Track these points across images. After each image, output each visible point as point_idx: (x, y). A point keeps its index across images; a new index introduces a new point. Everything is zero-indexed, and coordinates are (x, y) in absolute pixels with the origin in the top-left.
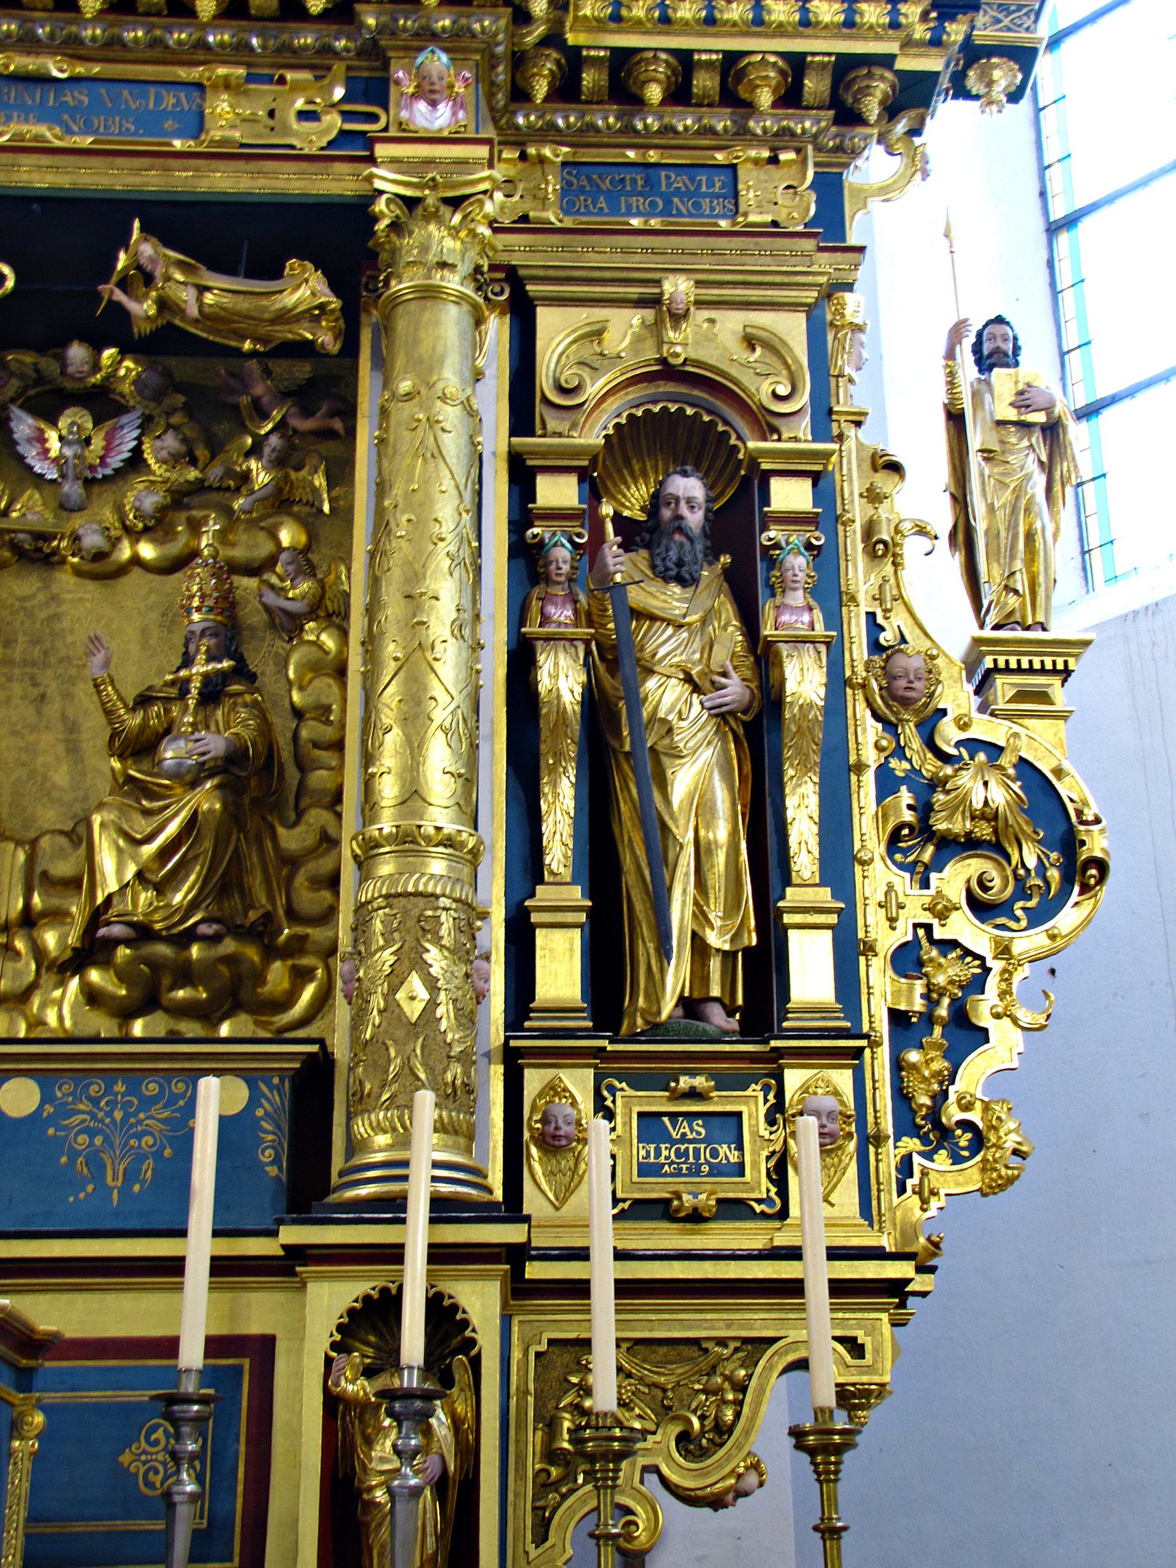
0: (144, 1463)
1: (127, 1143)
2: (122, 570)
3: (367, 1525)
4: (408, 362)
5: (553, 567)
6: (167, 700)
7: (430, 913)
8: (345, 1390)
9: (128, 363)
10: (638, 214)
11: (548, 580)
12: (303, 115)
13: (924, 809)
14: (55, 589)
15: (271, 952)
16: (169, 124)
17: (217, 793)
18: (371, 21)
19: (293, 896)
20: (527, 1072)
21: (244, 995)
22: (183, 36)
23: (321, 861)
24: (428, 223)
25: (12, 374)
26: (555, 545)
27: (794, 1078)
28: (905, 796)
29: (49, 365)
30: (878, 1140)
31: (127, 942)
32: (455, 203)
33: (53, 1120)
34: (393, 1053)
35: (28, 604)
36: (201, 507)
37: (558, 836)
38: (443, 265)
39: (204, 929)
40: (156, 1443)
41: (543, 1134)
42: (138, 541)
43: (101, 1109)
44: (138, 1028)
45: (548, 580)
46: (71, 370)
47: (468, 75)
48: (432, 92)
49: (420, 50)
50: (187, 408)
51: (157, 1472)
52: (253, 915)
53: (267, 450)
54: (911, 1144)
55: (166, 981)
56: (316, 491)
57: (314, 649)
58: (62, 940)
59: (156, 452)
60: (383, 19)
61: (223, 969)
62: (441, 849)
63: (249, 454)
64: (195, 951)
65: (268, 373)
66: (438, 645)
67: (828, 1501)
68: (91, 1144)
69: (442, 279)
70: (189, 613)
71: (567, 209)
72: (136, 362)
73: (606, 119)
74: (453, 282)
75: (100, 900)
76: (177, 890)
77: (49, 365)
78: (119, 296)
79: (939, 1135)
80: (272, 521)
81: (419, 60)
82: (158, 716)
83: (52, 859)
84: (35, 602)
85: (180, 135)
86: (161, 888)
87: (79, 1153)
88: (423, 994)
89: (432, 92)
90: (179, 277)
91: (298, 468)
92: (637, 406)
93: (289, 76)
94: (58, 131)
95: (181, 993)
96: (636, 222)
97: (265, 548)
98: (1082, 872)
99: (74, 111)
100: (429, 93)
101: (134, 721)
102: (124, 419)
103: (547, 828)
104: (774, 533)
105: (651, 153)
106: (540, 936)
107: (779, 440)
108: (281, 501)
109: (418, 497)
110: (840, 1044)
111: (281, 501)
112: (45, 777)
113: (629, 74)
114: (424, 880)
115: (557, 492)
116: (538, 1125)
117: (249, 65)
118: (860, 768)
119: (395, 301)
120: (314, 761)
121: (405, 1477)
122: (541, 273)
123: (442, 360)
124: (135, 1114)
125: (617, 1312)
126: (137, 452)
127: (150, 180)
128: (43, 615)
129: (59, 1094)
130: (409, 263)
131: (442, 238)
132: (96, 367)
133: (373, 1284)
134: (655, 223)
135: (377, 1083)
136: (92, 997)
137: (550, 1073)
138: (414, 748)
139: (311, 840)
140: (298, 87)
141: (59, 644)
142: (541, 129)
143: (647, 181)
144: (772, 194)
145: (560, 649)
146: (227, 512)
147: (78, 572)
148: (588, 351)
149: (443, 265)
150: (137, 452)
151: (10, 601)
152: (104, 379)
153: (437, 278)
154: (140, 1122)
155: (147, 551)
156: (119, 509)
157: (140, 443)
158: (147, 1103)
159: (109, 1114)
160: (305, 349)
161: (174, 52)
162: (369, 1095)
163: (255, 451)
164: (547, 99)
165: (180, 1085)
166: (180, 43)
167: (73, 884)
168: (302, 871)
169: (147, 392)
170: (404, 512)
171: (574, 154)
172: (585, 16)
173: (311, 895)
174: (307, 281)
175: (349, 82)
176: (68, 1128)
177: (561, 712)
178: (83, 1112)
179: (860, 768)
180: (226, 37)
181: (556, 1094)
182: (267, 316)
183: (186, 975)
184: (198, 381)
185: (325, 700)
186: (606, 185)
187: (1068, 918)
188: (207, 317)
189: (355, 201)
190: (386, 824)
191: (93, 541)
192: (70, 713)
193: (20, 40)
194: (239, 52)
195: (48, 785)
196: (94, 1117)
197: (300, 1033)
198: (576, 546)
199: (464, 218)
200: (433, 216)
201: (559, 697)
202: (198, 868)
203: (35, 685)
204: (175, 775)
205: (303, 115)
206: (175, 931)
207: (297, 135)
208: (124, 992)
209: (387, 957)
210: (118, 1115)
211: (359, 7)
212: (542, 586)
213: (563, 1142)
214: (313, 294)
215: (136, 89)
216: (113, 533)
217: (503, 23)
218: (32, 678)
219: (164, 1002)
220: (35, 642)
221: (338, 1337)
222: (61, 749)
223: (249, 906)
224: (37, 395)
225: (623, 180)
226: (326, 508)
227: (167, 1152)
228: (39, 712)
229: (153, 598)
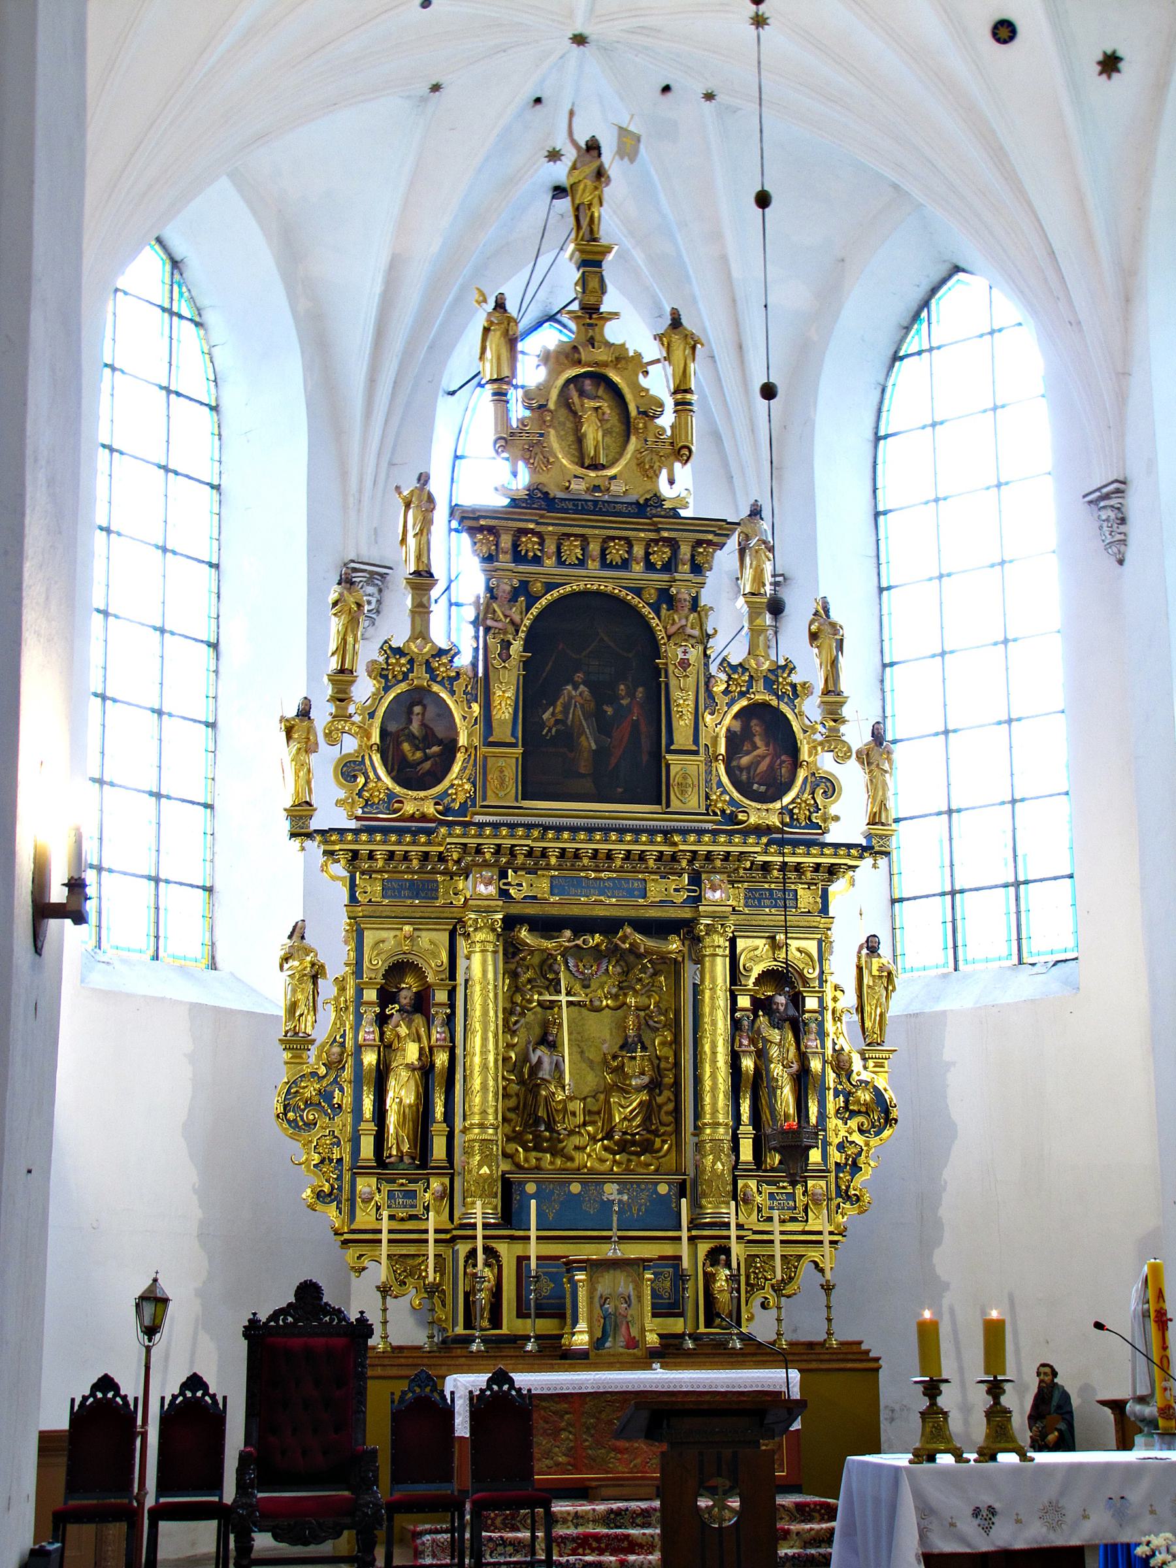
12: (676, 890)
13: (847, 1102)
27: (810, 1183)
28: (842, 1098)
30: (831, 1199)
54: (840, 1200)
67: (828, 1300)
74: (719, 951)
79: (848, 1198)
98: (889, 1121)
100: (714, 889)
103: (742, 1109)
104: (807, 1015)
110: (821, 1173)
118: (829, 1089)
127: (633, 913)
138: (714, 1098)
144: (806, 898)
158: (642, 1190)
179: (829, 1089)
187: (886, 1133)
190: (476, 1120)
205: (676, 890)
223: (652, 1124)
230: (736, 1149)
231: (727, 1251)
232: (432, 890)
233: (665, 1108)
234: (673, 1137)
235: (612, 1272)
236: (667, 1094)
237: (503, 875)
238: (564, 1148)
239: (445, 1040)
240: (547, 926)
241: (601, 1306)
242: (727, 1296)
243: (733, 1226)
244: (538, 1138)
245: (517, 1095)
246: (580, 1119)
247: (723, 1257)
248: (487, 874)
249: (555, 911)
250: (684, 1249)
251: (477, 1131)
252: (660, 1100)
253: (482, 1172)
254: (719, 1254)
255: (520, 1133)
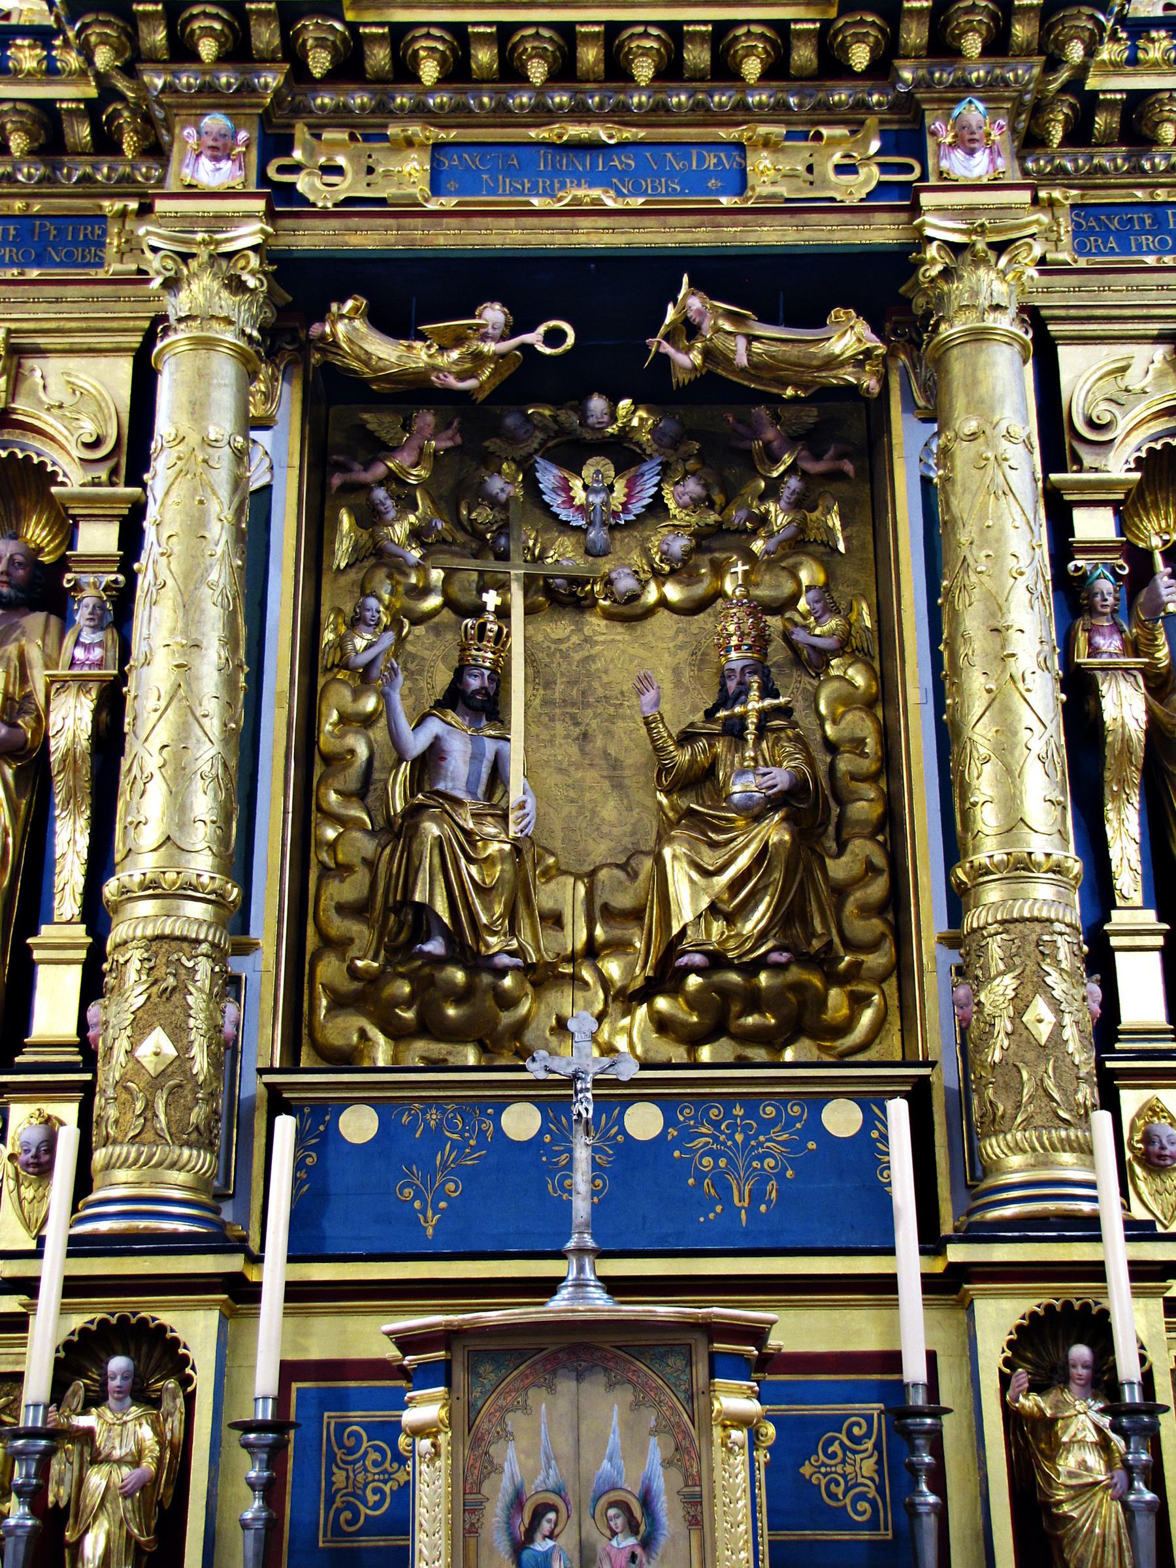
0: (825, 1475)
1: (750, 1165)
2: (650, 612)
3: (1060, 1539)
4: (969, 403)
5: (1098, 598)
6: (710, 736)
7: (1046, 938)
8: (1023, 1406)
9: (642, 413)
10: (1150, 252)
11: (1092, 611)
12: (840, 169)
14: (587, 631)
15: (834, 978)
16: (712, 183)
17: (785, 825)
18: (907, 75)
19: (845, 924)
20: (1123, 1093)
21: (808, 1019)
22: (724, 99)
23: (869, 890)
24: (977, 267)
25: (536, 427)
26: (1098, 577)
29: (570, 418)
31: (698, 971)
32: (1000, 248)
33: (677, 1143)
34: (1025, 1076)
35: (563, 647)
36: (723, 550)
37: (1125, 862)
38: (997, 308)
39: (775, 957)
40: (834, 1456)
41: (1146, 1153)
42: (664, 584)
43: (722, 1132)
44: (705, 1054)
45: (1092, 611)
46: (591, 421)
47: (1002, 122)
48: (972, 141)
49: (958, 101)
50: (701, 456)
51: (838, 1484)
52: (816, 944)
53: (786, 493)
55: (735, 1008)
56: (830, 531)
57: (844, 684)
58: (629, 970)
59: (677, 497)
60: (921, 73)
61: (791, 996)
62: (1051, 875)
63: (763, 497)
64: (763, 978)
65: (777, 418)
66: (1028, 675)
68: (716, 1165)
69: (995, 321)
70: (728, 651)
71: (1080, 249)
72: (649, 411)
73: (1075, 161)
75: (676, 929)
76: (746, 919)
77: (570, 418)
78: (667, 348)
80: (791, 561)
81: (956, 113)
82: (704, 751)
83: (613, 891)
84: (569, 644)
85: (724, 191)
86: (731, 919)
87: (705, 1175)
88: (1050, 1018)
89: (972, 141)
90: (728, 327)
91: (813, 509)
92: (1156, 440)
93: (825, 131)
94: (612, 193)
95: (750, 1020)
96: (1151, 260)
97: (788, 587)
99: (623, 174)
100: (966, 142)
101: (684, 757)
102: (645, 467)
103: (1114, 853)
105: (1159, 192)
106: (43, 972)
107: (1080, 471)
108: (799, 543)
109: (992, 534)
111: (799, 543)
112: (594, 813)
113: (1141, 117)
114: (1037, 906)
115: (1093, 525)
116: (1140, 1145)
117: (787, 123)
119: (946, 347)
120: (852, 792)
121: (1139, 1491)
122: (1062, 313)
123: (1002, 400)
124: (756, 1137)
125: (1169, 1330)
126: (658, 497)
128: (577, 656)
129: (681, 1118)
130: (961, 307)
131: (990, 284)
132: (614, 418)
133: (1038, 1301)
134: (34, 274)
135: (1010, 1105)
136: (662, 1024)
137: (1147, 1094)
138: (1010, 774)
139: (858, 868)
140: (834, 142)
141: (596, 684)
142: (1050, 173)
143: (1155, 221)
145: (1121, 678)
146: (749, 557)
147: (608, 615)
148: (1110, 387)
149: (997, 308)
150: (658, 497)
151: (547, 644)
152: (622, 429)
153: (991, 320)
154: (761, 1144)
155: (674, 592)
156: (646, 552)
157: (661, 489)
158: (766, 1125)
159: (731, 1137)
160: (852, 391)
161: (715, 114)
162: (1003, 1116)
163: (772, 491)
164: (1061, 145)
165: (796, 1108)
166: (721, 105)
167: (636, 915)
168: (852, 899)
169: (666, 440)
170: (981, 548)
171: (1082, 196)
172: (1103, 61)
173: (862, 923)
174: (852, 328)
175: (883, 135)
176: (691, 1150)
177: (1126, 741)
178: (705, 1135)
180: (764, 98)
181: (1155, 1113)
182: (815, 363)
183: (754, 1001)
184: (716, 425)
185: (860, 734)
186: (1115, 225)
188: (757, 367)
189: (897, 249)
191: (626, 583)
192: (612, 750)
193: (572, 110)
194: (778, 112)
195: (597, 820)
196: (716, 1139)
197: (860, 1058)
198: (1118, 577)
199: (1010, 261)
200: (979, 261)
201: (1123, 726)
202: (767, 899)
203: (577, 724)
204: (741, 809)
205: (840, 169)
206: (745, 959)
207: (836, 187)
208: (695, 1019)
209: (1006, 984)
210: (739, 1137)
211: (897, 63)
212: (1087, 617)
213: (1169, 1162)
214: (859, 340)
215: (680, 151)
216: (642, 576)
217: (1036, 71)
218: (573, 717)
219: (733, 1026)
220: (571, 683)
221: (1009, 1354)
222: (606, 785)
223: (811, 934)
224: (554, 447)
225: (1131, 220)
226: (841, 547)
227: (789, 1173)
228: (582, 750)
229: (681, 637)
230: (1100, 961)
231: (1097, 1328)
232: (87, 243)
233: (857, 896)
234: (891, 986)
235: (566, 1386)
236: (862, 849)
237: (274, 143)
238: (522, 1024)
239: (100, 664)
240: (412, 292)
241: (519, 1547)
242: (1111, 1511)
243: (1113, 1227)
244: (427, 990)
245: (371, 864)
246: (576, 936)
247: (1080, 1352)
248: (216, 121)
249: (446, 238)
250: (913, 1328)
251: (147, 907)
252: (839, 868)
253: (145, 1052)
254: (1061, 1340)
255: (374, 980)
